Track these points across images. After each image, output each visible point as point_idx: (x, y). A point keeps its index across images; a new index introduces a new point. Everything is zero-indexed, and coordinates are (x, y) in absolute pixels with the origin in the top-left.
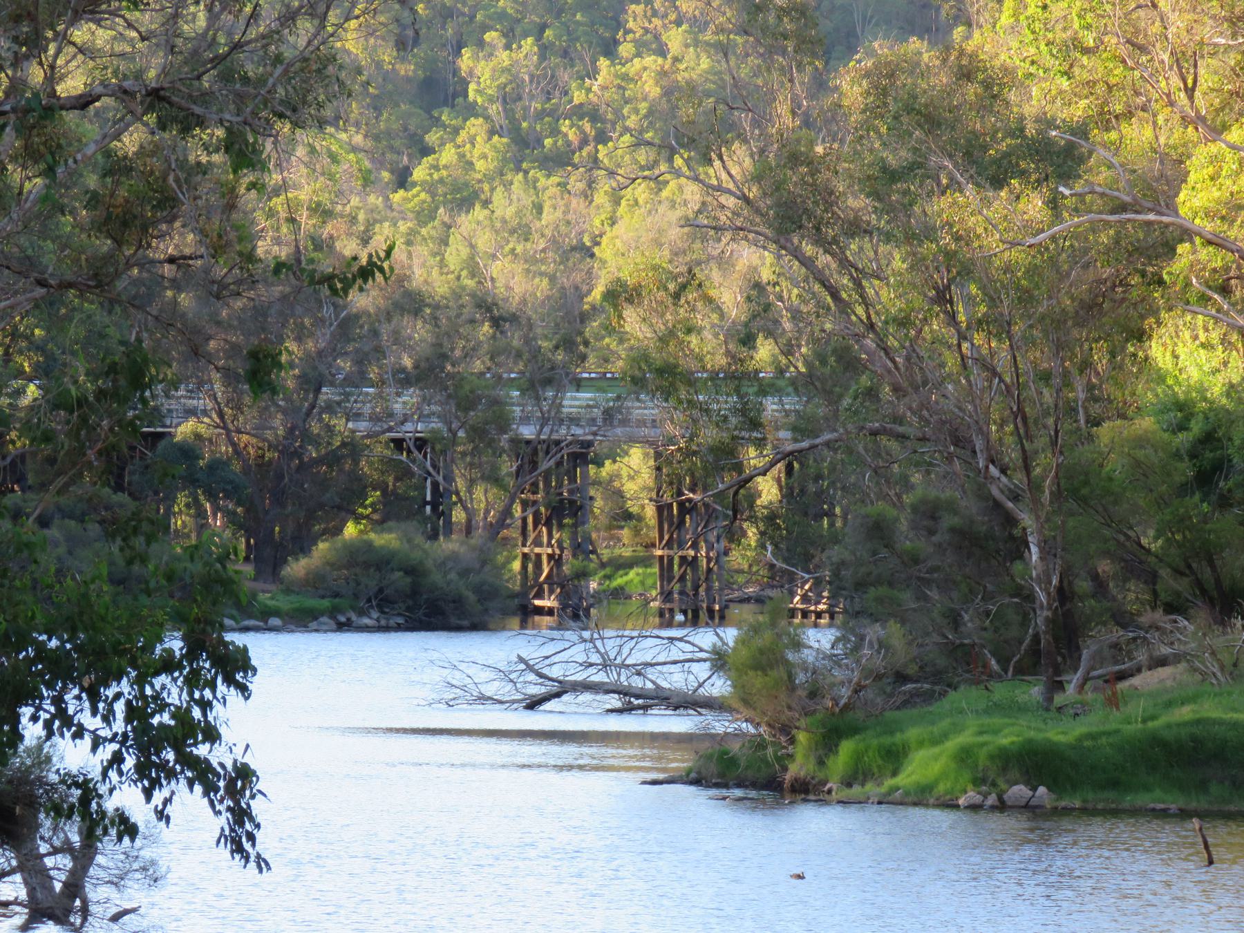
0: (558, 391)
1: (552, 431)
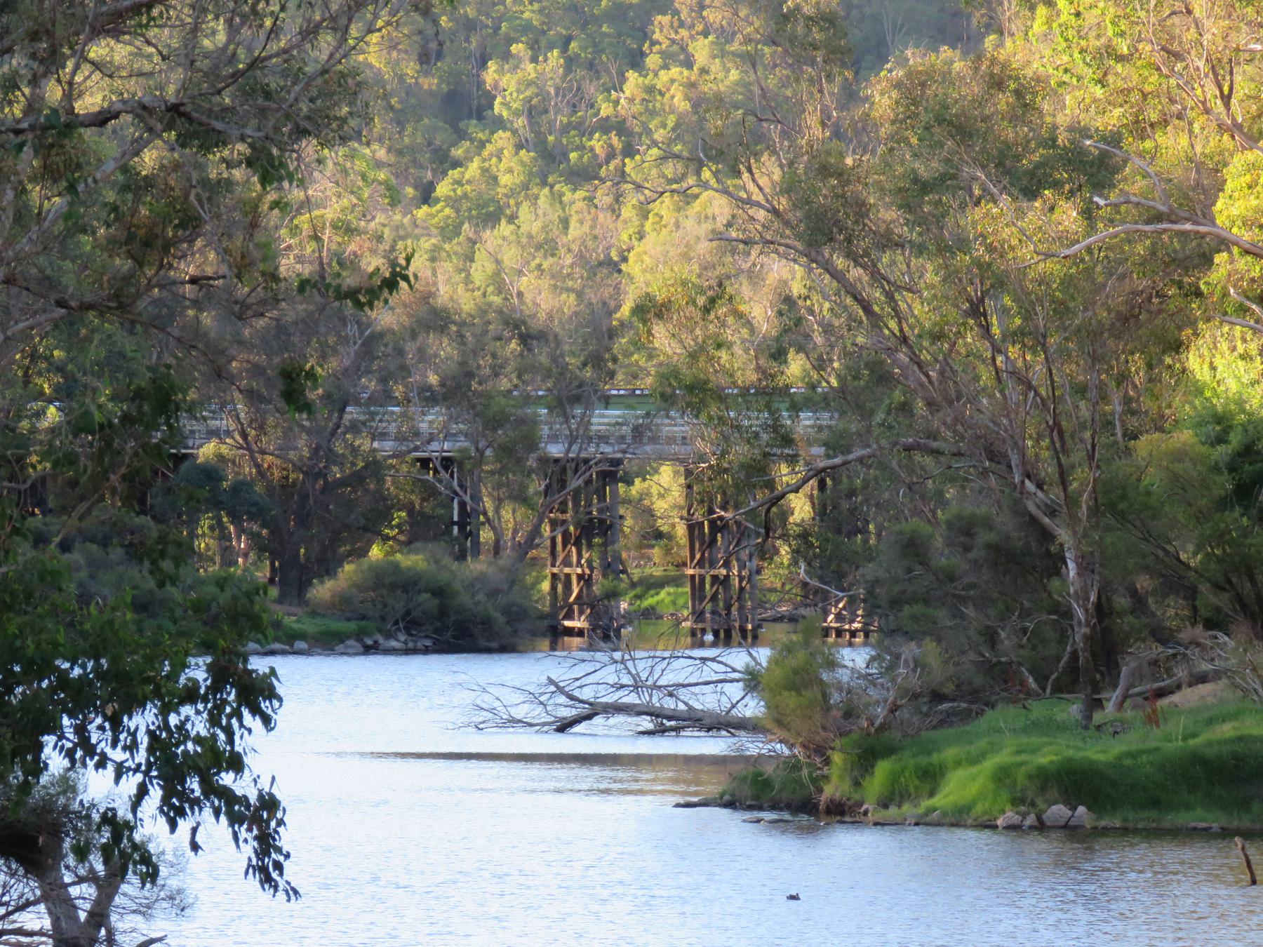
1: (581, 449)
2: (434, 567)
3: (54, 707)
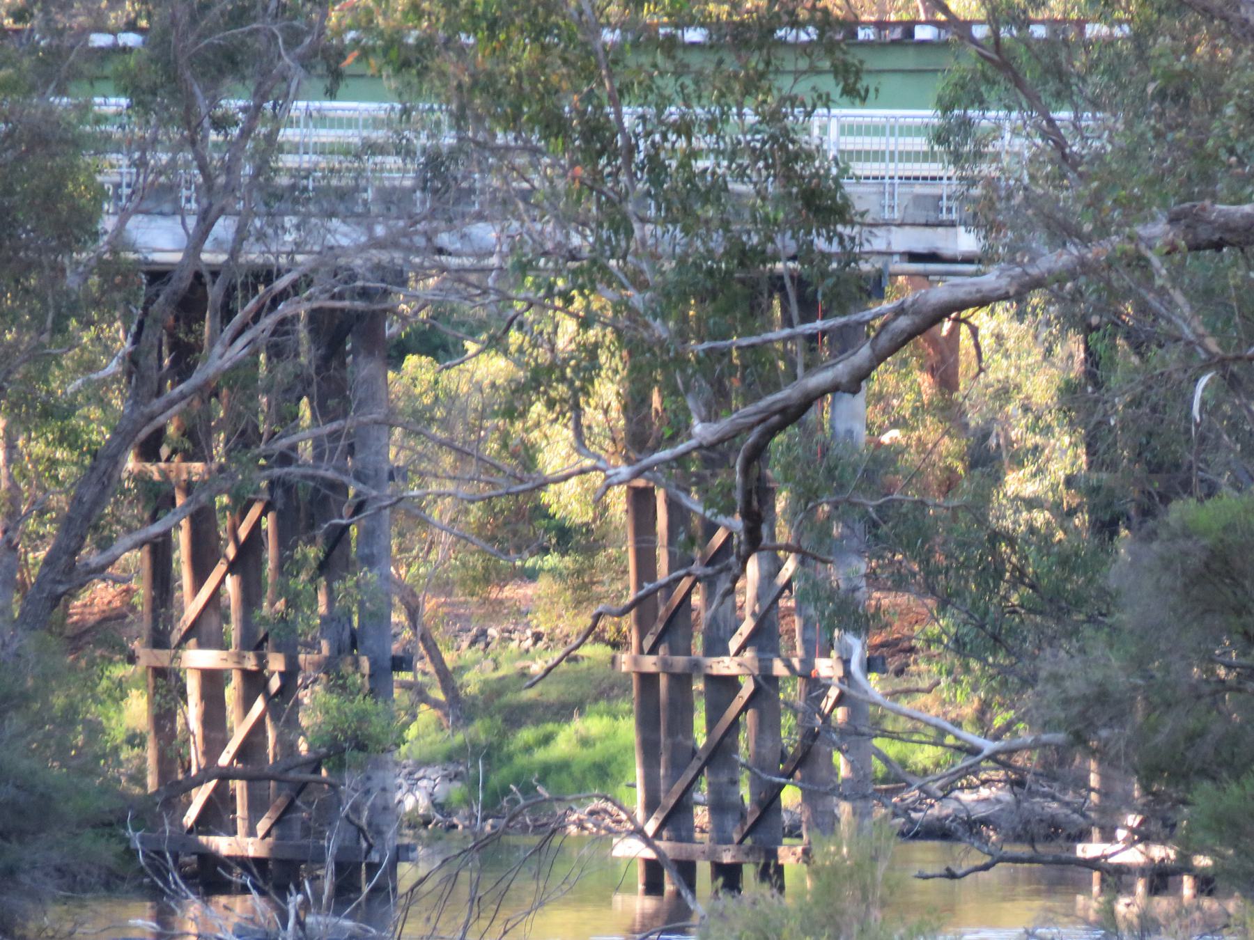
0: (261, 95)
1: (241, 235)
2: (1220, 861)
3: (1071, 582)
